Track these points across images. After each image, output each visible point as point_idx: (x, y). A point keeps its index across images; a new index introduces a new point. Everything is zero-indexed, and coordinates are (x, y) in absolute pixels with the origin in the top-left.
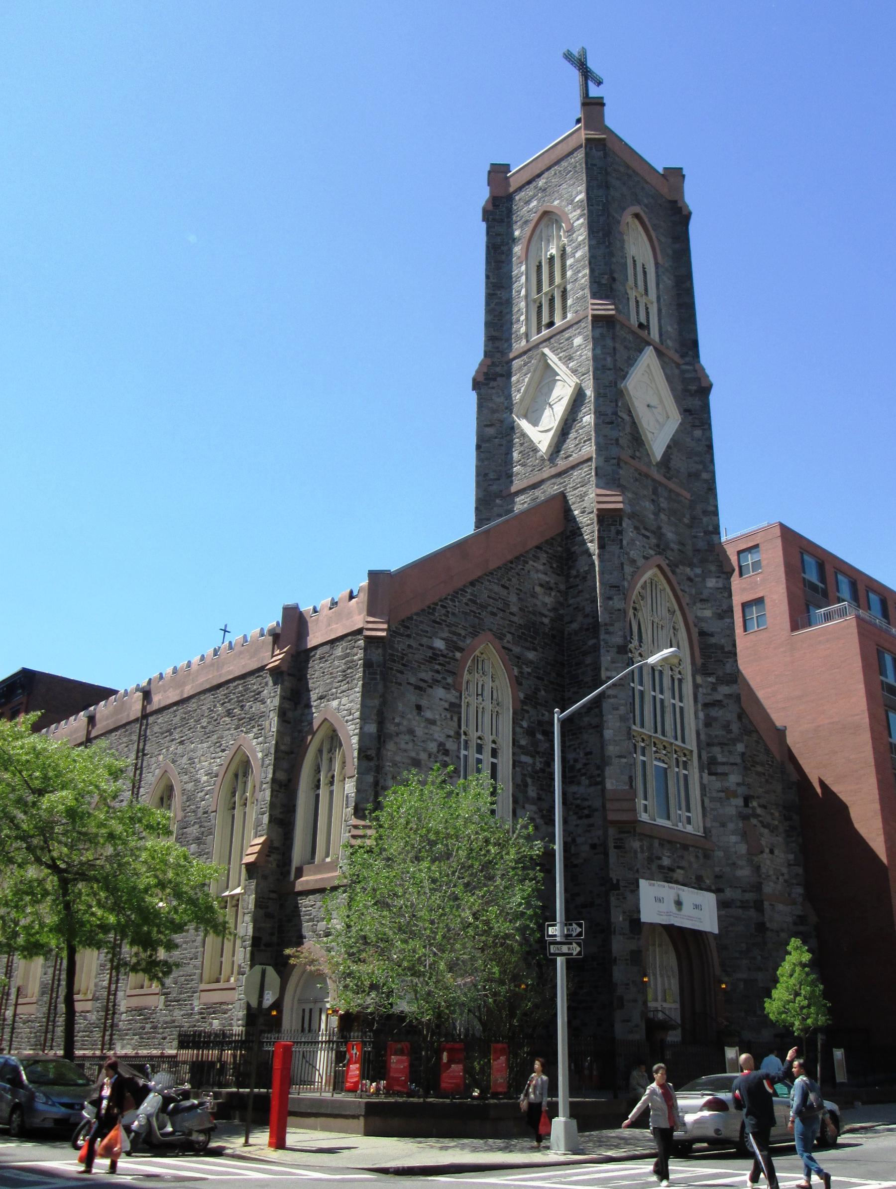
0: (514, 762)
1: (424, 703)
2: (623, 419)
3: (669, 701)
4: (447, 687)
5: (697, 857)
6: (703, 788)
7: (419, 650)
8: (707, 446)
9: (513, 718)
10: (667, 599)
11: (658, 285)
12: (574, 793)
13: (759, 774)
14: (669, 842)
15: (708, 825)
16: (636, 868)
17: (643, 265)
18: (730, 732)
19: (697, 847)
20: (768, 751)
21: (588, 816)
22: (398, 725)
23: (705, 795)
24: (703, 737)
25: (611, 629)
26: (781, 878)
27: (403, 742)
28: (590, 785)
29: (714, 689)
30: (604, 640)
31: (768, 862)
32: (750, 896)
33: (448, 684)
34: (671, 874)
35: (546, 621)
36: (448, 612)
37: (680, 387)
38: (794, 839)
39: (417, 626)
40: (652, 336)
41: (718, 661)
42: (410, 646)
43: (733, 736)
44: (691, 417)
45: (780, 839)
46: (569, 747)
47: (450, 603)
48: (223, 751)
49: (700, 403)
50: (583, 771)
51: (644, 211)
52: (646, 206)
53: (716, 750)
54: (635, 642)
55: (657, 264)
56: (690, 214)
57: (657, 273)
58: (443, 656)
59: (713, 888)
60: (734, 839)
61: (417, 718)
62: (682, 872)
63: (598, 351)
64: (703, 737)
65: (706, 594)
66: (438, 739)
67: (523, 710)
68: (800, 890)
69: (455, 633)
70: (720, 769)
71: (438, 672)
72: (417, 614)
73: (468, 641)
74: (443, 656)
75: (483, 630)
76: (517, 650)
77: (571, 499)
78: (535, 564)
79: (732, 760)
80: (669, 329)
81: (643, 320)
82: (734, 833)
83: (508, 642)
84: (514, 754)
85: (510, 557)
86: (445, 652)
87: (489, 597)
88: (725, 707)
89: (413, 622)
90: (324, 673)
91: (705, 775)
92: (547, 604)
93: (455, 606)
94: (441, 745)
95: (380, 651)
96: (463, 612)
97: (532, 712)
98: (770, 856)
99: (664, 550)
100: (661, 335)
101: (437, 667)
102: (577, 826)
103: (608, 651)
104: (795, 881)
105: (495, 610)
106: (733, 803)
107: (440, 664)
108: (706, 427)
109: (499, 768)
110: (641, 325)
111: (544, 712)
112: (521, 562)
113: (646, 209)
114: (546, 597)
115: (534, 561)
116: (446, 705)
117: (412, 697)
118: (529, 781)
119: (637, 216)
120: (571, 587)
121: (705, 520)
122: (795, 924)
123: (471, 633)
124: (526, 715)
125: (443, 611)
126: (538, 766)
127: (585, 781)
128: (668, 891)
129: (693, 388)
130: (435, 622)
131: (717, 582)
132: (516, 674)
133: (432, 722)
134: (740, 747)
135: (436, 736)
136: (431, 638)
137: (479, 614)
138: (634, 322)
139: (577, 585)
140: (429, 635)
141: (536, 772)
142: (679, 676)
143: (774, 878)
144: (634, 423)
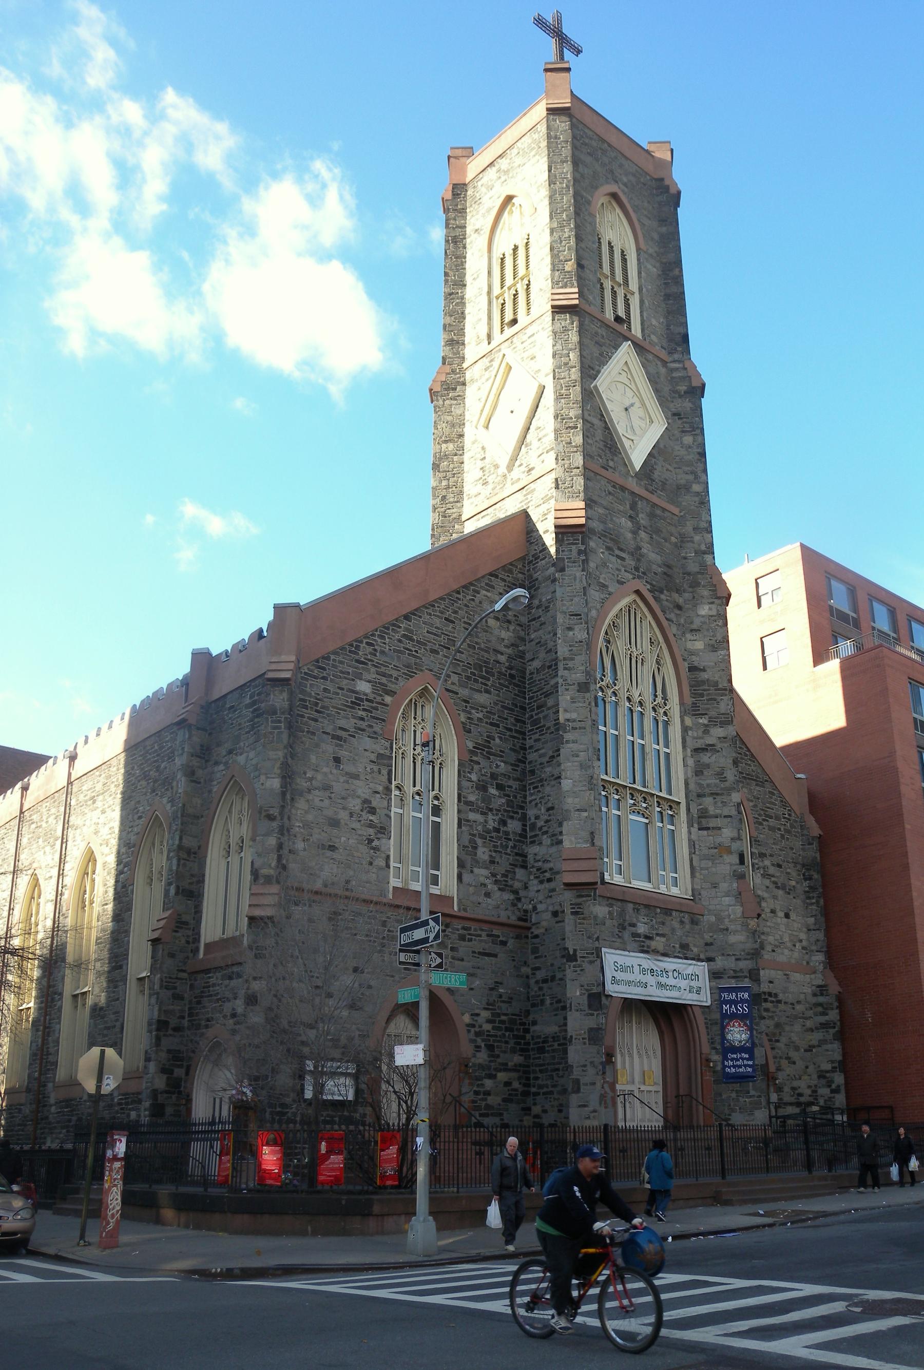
0: (460, 820)
1: (343, 753)
2: (593, 424)
3: (652, 747)
4: (374, 736)
5: (682, 922)
6: (692, 845)
7: (338, 694)
8: (699, 453)
9: (459, 771)
10: (647, 628)
11: (639, 273)
12: (535, 854)
13: (772, 829)
14: (647, 906)
15: (697, 887)
16: (596, 936)
17: (623, 252)
18: (724, 780)
19: (682, 912)
20: (784, 804)
21: (549, 880)
22: (311, 779)
23: (694, 853)
24: (692, 786)
25: (570, 664)
26: (798, 945)
27: (317, 800)
28: (552, 845)
29: (706, 732)
30: (562, 677)
31: (783, 928)
32: (745, 965)
33: (375, 733)
34: (648, 942)
35: (502, 658)
36: (375, 650)
37: (666, 389)
38: (814, 901)
39: (334, 666)
40: (633, 332)
41: (711, 699)
42: (325, 690)
43: (727, 784)
44: (680, 422)
45: (798, 902)
46: (530, 802)
47: (379, 640)
48: (140, 817)
49: (690, 405)
50: (545, 829)
51: (623, 191)
52: (625, 185)
53: (708, 801)
54: (609, 679)
55: (638, 249)
56: (679, 193)
57: (638, 260)
58: (367, 700)
59: (702, 956)
60: (726, 900)
61: (335, 771)
62: (663, 939)
63: (559, 347)
64: (692, 786)
65: (697, 623)
66: (362, 795)
67: (472, 761)
68: (820, 957)
69: (384, 675)
70: (712, 823)
71: (362, 719)
72: (335, 653)
73: (402, 683)
74: (367, 700)
75: (422, 670)
76: (464, 692)
77: (534, 517)
78: (489, 594)
79: (726, 813)
80: (654, 322)
81: (621, 313)
82: (727, 895)
83: (453, 684)
84: (459, 811)
85: (455, 587)
86: (371, 697)
87: (428, 632)
88: (718, 751)
89: (331, 662)
90: (232, 724)
91: (694, 830)
92: (503, 639)
93: (385, 643)
94: (366, 801)
95: (285, 695)
96: (395, 651)
97: (483, 763)
98: (786, 920)
99: (644, 573)
100: (643, 330)
101: (361, 713)
102: (538, 891)
103: (567, 690)
104: (814, 948)
105: (436, 647)
106: (728, 861)
107: (364, 710)
108: (698, 431)
109: (443, 828)
110: (618, 319)
111: (499, 763)
112: (471, 592)
113: (626, 189)
114: (503, 632)
115: (488, 591)
116: (373, 757)
117: (329, 748)
118: (479, 841)
119: (614, 196)
120: (534, 619)
121: (697, 538)
122: (815, 995)
123: (404, 673)
124: (476, 767)
125: (370, 649)
126: (491, 825)
127: (546, 840)
128: (636, 959)
129: (682, 388)
130: (358, 661)
131: (710, 609)
132: (463, 720)
133: (356, 777)
134: (736, 797)
135: (360, 792)
136: (353, 680)
137: (416, 651)
138: (609, 315)
139: (540, 617)
140: (350, 677)
141: (488, 832)
142: (665, 718)
143: (789, 944)
144: (607, 428)
